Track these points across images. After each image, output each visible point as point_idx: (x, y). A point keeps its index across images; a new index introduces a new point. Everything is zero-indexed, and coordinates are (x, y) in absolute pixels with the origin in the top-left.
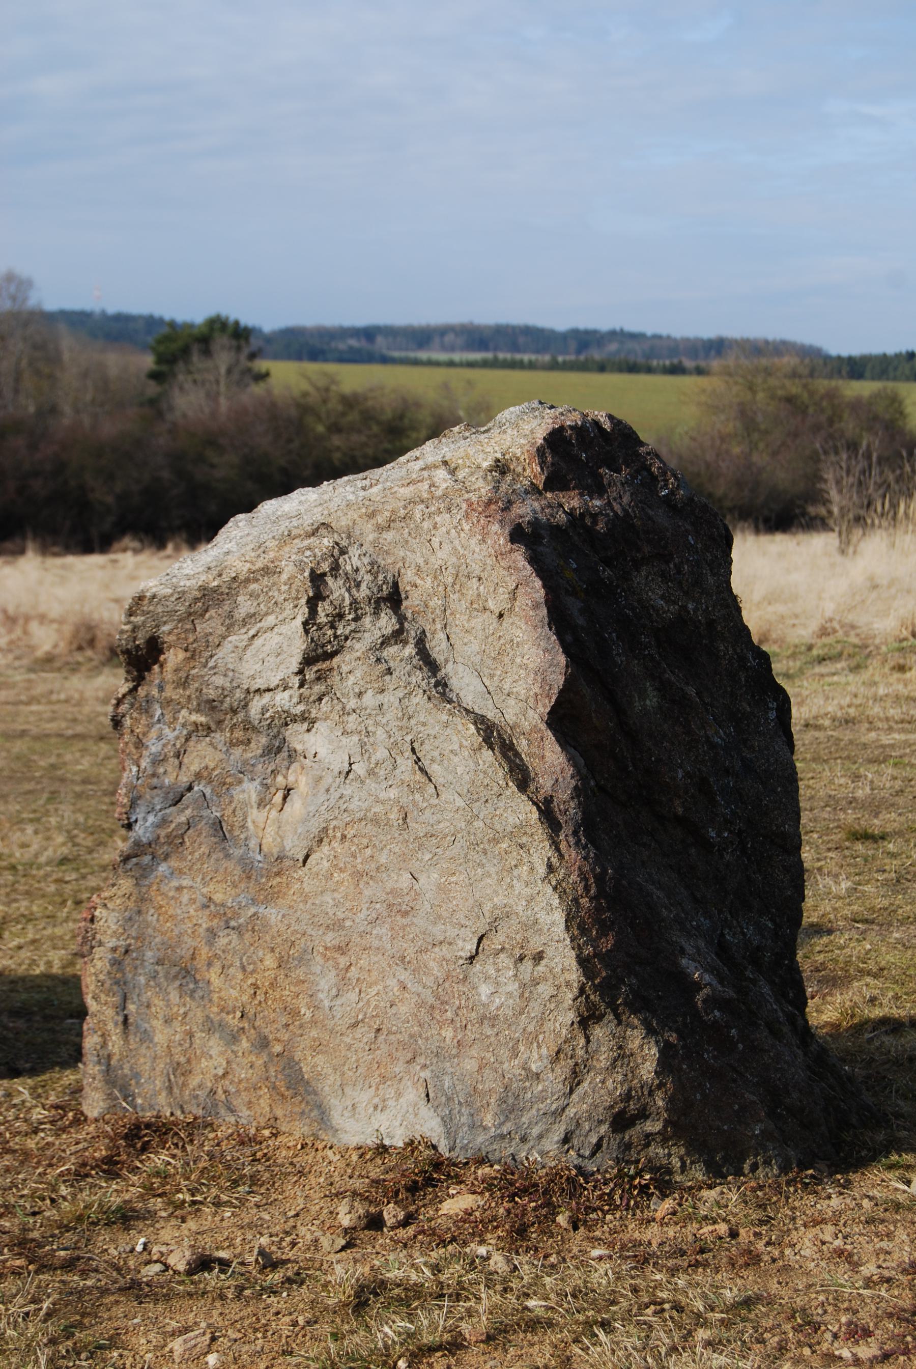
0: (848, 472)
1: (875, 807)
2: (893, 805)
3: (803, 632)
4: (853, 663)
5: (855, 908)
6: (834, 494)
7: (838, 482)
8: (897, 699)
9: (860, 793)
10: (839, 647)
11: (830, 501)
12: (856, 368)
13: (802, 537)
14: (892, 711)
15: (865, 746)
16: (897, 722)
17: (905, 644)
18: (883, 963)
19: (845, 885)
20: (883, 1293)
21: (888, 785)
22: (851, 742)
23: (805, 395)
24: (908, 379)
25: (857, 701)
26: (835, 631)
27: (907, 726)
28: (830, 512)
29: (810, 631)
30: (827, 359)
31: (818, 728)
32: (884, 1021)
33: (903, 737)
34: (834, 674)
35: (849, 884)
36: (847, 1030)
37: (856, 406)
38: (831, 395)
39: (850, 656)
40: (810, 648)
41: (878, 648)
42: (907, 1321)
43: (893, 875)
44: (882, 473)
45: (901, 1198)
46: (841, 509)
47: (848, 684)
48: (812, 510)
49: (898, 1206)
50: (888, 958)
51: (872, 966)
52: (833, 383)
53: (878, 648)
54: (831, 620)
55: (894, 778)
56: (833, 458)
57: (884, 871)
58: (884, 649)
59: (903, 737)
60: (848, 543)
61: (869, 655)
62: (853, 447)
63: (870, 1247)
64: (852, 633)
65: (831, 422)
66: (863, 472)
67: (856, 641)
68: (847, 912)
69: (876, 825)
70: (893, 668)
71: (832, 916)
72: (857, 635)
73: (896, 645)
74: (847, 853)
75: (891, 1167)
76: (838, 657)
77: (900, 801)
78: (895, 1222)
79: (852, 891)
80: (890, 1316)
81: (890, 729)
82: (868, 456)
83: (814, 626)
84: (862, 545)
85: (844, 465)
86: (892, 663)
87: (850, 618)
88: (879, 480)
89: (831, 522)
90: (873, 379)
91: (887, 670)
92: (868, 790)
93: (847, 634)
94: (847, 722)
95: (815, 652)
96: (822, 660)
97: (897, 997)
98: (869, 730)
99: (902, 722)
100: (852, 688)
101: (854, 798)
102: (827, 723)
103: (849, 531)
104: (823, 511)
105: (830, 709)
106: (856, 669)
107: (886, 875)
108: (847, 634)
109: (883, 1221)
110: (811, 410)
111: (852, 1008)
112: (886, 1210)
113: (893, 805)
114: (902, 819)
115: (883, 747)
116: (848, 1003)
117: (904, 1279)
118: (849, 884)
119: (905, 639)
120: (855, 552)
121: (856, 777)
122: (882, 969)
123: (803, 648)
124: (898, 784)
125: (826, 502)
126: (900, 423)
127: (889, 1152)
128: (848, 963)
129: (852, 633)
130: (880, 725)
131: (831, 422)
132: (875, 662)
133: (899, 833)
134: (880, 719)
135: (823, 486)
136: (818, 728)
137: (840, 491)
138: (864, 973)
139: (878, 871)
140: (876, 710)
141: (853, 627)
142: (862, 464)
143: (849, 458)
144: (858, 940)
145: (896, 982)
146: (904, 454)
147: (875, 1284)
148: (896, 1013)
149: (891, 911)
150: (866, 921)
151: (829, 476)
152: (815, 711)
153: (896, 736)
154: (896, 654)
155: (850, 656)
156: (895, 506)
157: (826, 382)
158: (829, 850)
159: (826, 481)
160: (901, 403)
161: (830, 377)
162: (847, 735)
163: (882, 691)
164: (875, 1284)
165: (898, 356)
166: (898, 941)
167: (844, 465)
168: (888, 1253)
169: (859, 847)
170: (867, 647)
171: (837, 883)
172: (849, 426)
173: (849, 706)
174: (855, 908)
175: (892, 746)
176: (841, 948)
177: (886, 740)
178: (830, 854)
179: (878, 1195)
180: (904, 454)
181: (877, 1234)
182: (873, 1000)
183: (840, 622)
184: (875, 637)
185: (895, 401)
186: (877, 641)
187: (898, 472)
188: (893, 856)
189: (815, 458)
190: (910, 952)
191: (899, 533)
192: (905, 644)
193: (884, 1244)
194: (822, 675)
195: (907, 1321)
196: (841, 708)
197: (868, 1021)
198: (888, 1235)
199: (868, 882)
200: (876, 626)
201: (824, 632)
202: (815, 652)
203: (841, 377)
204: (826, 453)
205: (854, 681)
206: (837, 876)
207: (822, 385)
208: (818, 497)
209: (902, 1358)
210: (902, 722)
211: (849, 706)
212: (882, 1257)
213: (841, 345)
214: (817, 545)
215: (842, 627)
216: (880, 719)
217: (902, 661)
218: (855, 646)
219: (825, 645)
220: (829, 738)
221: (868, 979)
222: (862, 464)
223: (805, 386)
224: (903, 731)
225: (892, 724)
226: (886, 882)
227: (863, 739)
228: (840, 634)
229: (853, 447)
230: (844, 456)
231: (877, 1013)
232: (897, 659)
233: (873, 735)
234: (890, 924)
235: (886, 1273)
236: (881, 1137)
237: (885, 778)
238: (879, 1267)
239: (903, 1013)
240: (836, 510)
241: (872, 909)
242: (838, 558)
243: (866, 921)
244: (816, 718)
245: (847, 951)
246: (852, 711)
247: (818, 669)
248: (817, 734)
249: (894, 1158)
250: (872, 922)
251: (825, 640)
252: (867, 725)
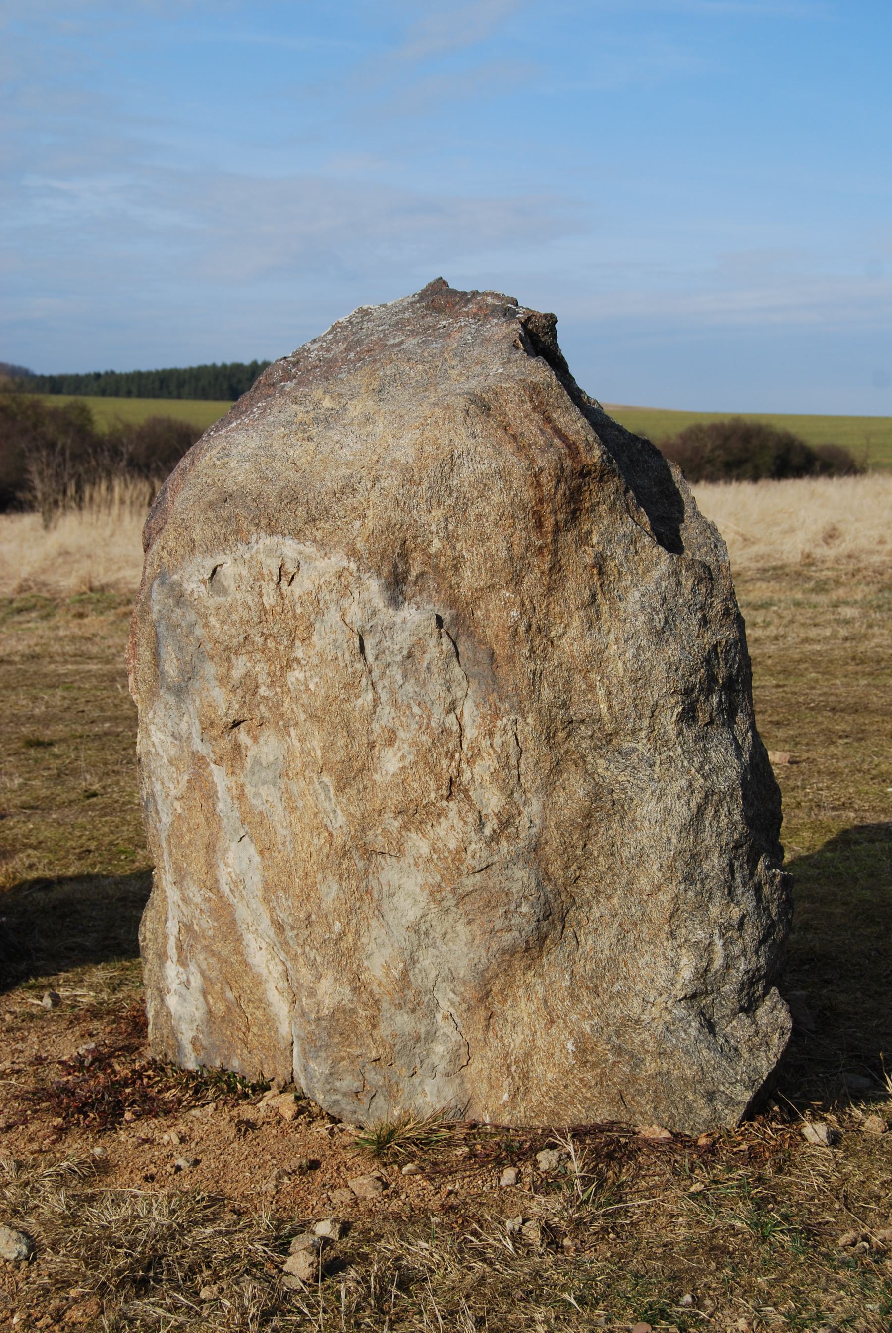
0: (48, 465)
1: (47, 721)
2: (61, 719)
3: (6, 590)
4: (44, 612)
5: (24, 798)
6: (37, 483)
7: (40, 473)
8: (73, 639)
9: (37, 711)
10: (33, 601)
11: (34, 489)
12: (56, 384)
13: (15, 517)
14: (68, 648)
15: (45, 675)
16: (71, 656)
17: (84, 597)
18: (41, 838)
19: (18, 781)
20: (13, 1082)
21: (59, 704)
22: (35, 673)
23: (14, 405)
24: (96, 394)
25: (43, 641)
26: (30, 588)
27: (79, 659)
28: (35, 497)
29: (11, 589)
30: (33, 377)
31: (10, 663)
32: (38, 881)
33: (74, 667)
34: (29, 622)
35: (21, 780)
36: (10, 890)
37: (54, 414)
38: (35, 406)
39: (43, 607)
40: (11, 601)
41: (63, 600)
42: (30, 1099)
43: (55, 771)
44: (73, 466)
45: (34, 1010)
46: (44, 494)
47: (37, 628)
48: (20, 495)
49: (32, 1017)
50: (46, 833)
51: (33, 840)
52: (36, 397)
53: (63, 600)
54: (26, 580)
55: (64, 698)
56: (35, 455)
57: (49, 769)
58: (68, 601)
59: (74, 667)
60: (50, 518)
61: (57, 606)
62: (51, 446)
63: (9, 1049)
64: (44, 589)
65: (35, 426)
66: (59, 465)
67: (46, 595)
68: (17, 801)
69: (47, 734)
70: (75, 616)
71: (5, 806)
72: (48, 591)
73: (77, 598)
74: (22, 757)
75: (31, 988)
76: (33, 608)
77: (67, 716)
78: (29, 1029)
79: (21, 786)
80: (16, 1097)
81: (66, 662)
82: (63, 452)
83: (15, 584)
84: (61, 521)
85: (44, 460)
86: (73, 612)
87: (42, 577)
88: (72, 472)
89: (36, 504)
90: (69, 394)
91: (69, 617)
92: (43, 709)
93: (40, 591)
94: (33, 657)
95: (15, 605)
96: (20, 611)
97: (50, 863)
98: (50, 663)
99: (75, 656)
100: (40, 632)
101: (33, 716)
102: (17, 659)
103: (50, 510)
104: (29, 496)
105: (20, 648)
106: (46, 617)
107: (50, 772)
108: (40, 591)
109: (19, 1029)
110: (19, 418)
111: (13, 873)
112: (23, 1021)
113: (61, 719)
114: (68, 729)
115: (59, 675)
116: (11, 870)
117: (30, 1069)
118: (21, 780)
119: (85, 593)
120: (55, 527)
121: (35, 699)
122: (40, 843)
123: (6, 602)
124: (67, 703)
125: (32, 489)
126: (89, 428)
127: (28, 978)
128: (14, 840)
129: (44, 589)
130: (58, 659)
131: (35, 426)
132: (61, 611)
133: (63, 740)
134: (58, 654)
135: (28, 476)
136: (10, 663)
137: (42, 480)
138: (26, 846)
139: (44, 769)
140: (56, 648)
141: (44, 585)
142: (59, 459)
143: (48, 455)
144: (24, 822)
145: (51, 851)
146: (90, 451)
147: (8, 1075)
148: (48, 874)
149: (51, 798)
150: (32, 807)
151: (33, 468)
152: (8, 649)
153: (70, 667)
154: (77, 605)
155: (43, 607)
156: (79, 489)
157: (30, 396)
158: (9, 755)
159: (30, 473)
160: (89, 412)
161: (32, 391)
162: (32, 667)
163: (62, 633)
164: (8, 1075)
165: (88, 376)
166: (55, 821)
167: (44, 460)
168: (22, 1052)
169: (32, 752)
170: (54, 599)
171: (12, 780)
172: (50, 430)
173: (36, 645)
174: (24, 798)
175: (66, 675)
176: (11, 829)
177: (62, 670)
178: (10, 759)
179: (18, 1010)
180: (90, 451)
181: (14, 1039)
182: (31, 866)
183: (34, 581)
184: (61, 592)
185: (84, 411)
186: (63, 595)
187: (86, 465)
188: (57, 757)
189: (22, 455)
190: (62, 829)
191: (85, 512)
192: (84, 597)
193: (19, 1046)
194: (20, 623)
195: (30, 1099)
196: (29, 647)
197: (26, 882)
198: (22, 1039)
199: (35, 778)
200: (62, 584)
201: (21, 589)
202: (15, 605)
203: (42, 392)
204: (30, 451)
205: (42, 627)
206: (11, 775)
207: (28, 398)
208: (24, 485)
209: (21, 1127)
210: (75, 656)
211: (36, 645)
212: (16, 1055)
213: (45, 365)
214: (28, 522)
215: (36, 585)
216: (58, 654)
217: (81, 610)
218: (46, 599)
219: (22, 599)
220: (19, 670)
221: (30, 851)
222: (59, 459)
223: (14, 399)
224: (76, 663)
225: (67, 657)
226: (49, 778)
227: (45, 670)
228: (35, 590)
229: (51, 446)
230: (44, 453)
231: (34, 875)
232: (78, 608)
233: (53, 666)
234: (50, 808)
235: (17, 1067)
236: (23, 966)
237: (58, 698)
238: (13, 1063)
239: (52, 874)
240: (39, 495)
241: (37, 798)
242: (42, 532)
243: (32, 807)
244: (9, 655)
245: (15, 831)
246: (38, 649)
247: (17, 618)
248: (9, 668)
249: (32, 981)
250: (36, 808)
251: (23, 595)
252: (48, 659)
